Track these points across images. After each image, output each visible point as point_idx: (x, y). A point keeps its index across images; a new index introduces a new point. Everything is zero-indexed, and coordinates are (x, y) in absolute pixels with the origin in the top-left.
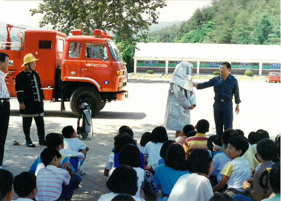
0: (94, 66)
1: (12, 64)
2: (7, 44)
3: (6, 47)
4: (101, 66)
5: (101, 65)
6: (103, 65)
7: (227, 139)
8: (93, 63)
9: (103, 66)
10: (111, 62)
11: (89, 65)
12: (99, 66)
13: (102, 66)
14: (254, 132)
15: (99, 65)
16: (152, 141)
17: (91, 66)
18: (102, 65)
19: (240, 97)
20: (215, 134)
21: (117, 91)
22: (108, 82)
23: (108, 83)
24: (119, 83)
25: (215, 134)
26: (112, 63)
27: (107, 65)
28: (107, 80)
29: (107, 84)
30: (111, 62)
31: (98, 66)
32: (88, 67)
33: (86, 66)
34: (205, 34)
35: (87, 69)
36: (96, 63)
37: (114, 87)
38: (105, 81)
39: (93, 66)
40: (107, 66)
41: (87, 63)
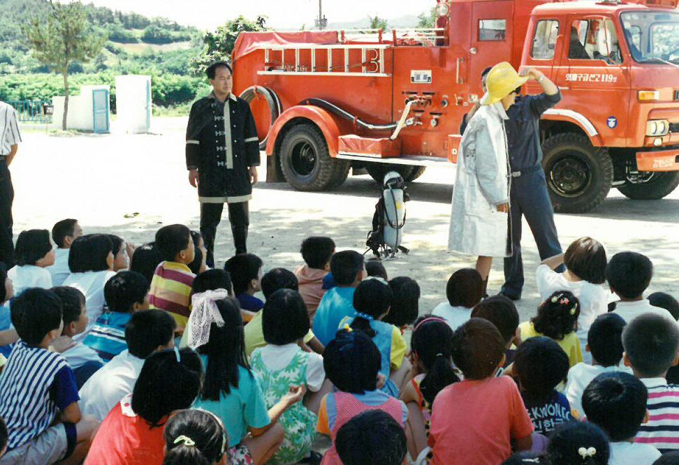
0: (584, 80)
1: (429, 78)
2: (439, 33)
3: (438, 40)
4: (600, 79)
5: (601, 77)
6: (605, 77)
7: (149, 396)
8: (584, 72)
9: (606, 79)
10: (625, 68)
11: (573, 77)
12: (597, 80)
13: (603, 80)
14: (447, 327)
15: (596, 77)
16: (325, 361)
17: (578, 79)
18: (603, 76)
19: (364, 198)
20: (454, 328)
21: (640, 144)
22: (616, 122)
23: (616, 124)
24: (649, 122)
25: (454, 328)
26: (627, 70)
27: (614, 76)
28: (614, 116)
29: (614, 127)
30: (625, 68)
31: (594, 79)
32: (570, 84)
33: (567, 79)
34: (69, 12)
35: (567, 88)
36: (590, 72)
37: (631, 133)
38: (610, 119)
39: (582, 79)
40: (615, 78)
41: (569, 71)
